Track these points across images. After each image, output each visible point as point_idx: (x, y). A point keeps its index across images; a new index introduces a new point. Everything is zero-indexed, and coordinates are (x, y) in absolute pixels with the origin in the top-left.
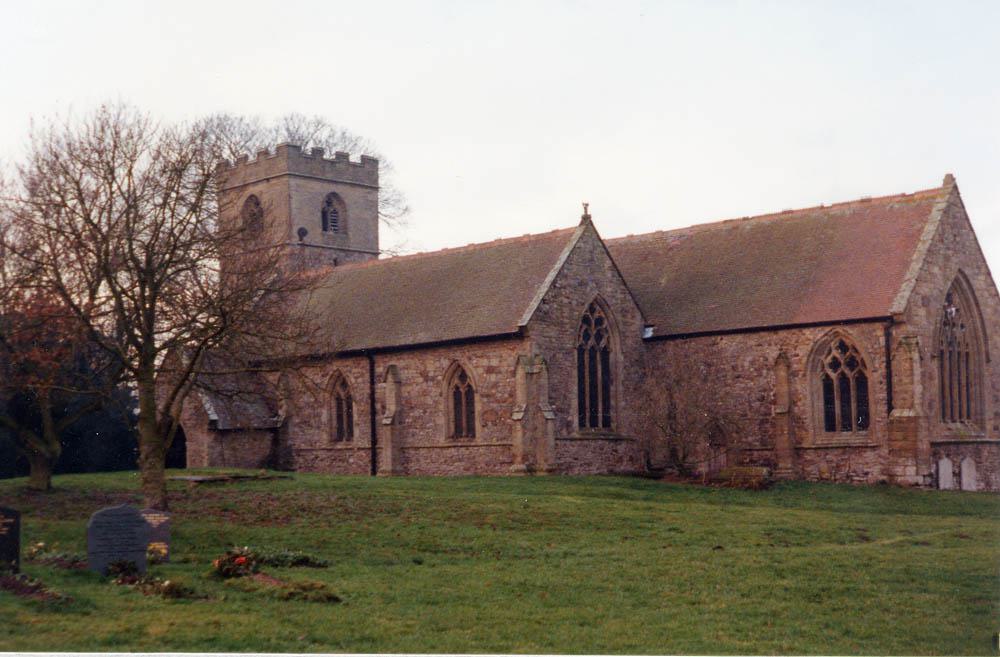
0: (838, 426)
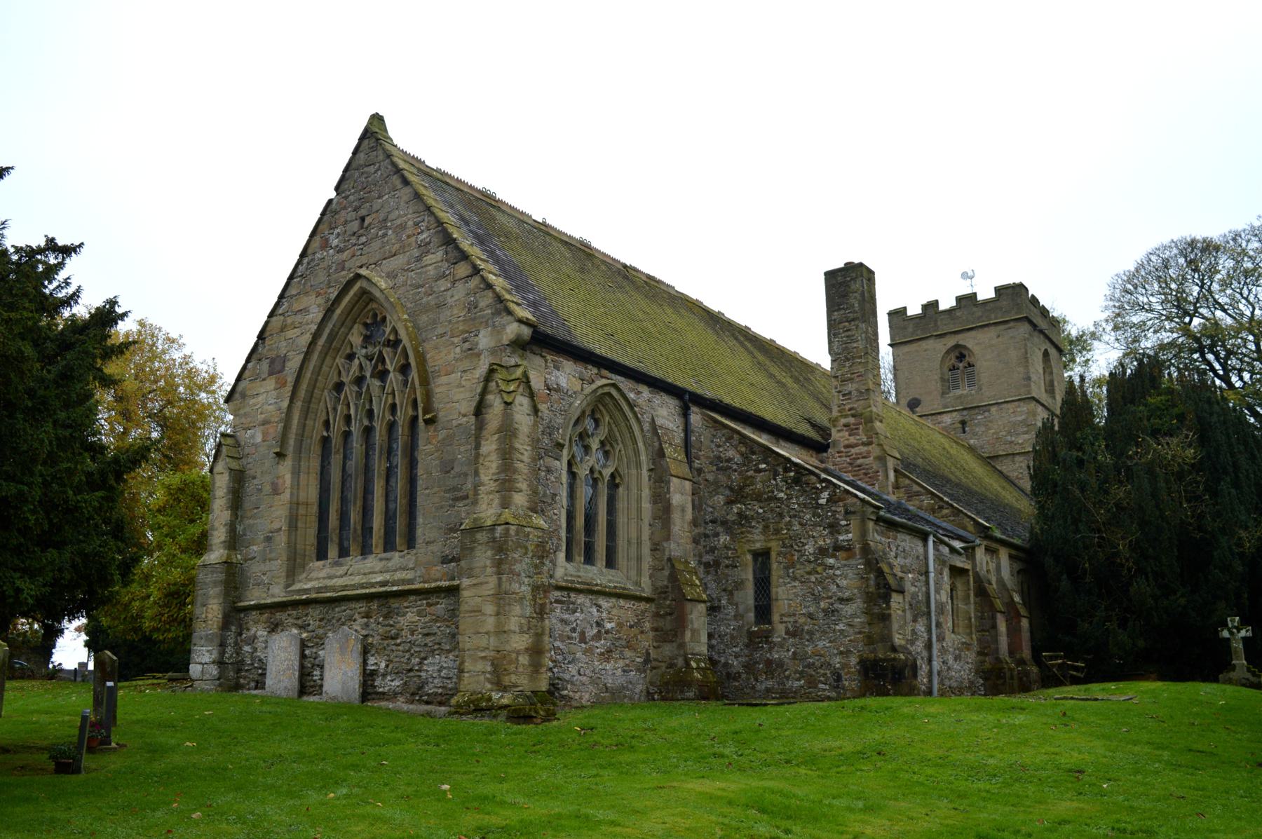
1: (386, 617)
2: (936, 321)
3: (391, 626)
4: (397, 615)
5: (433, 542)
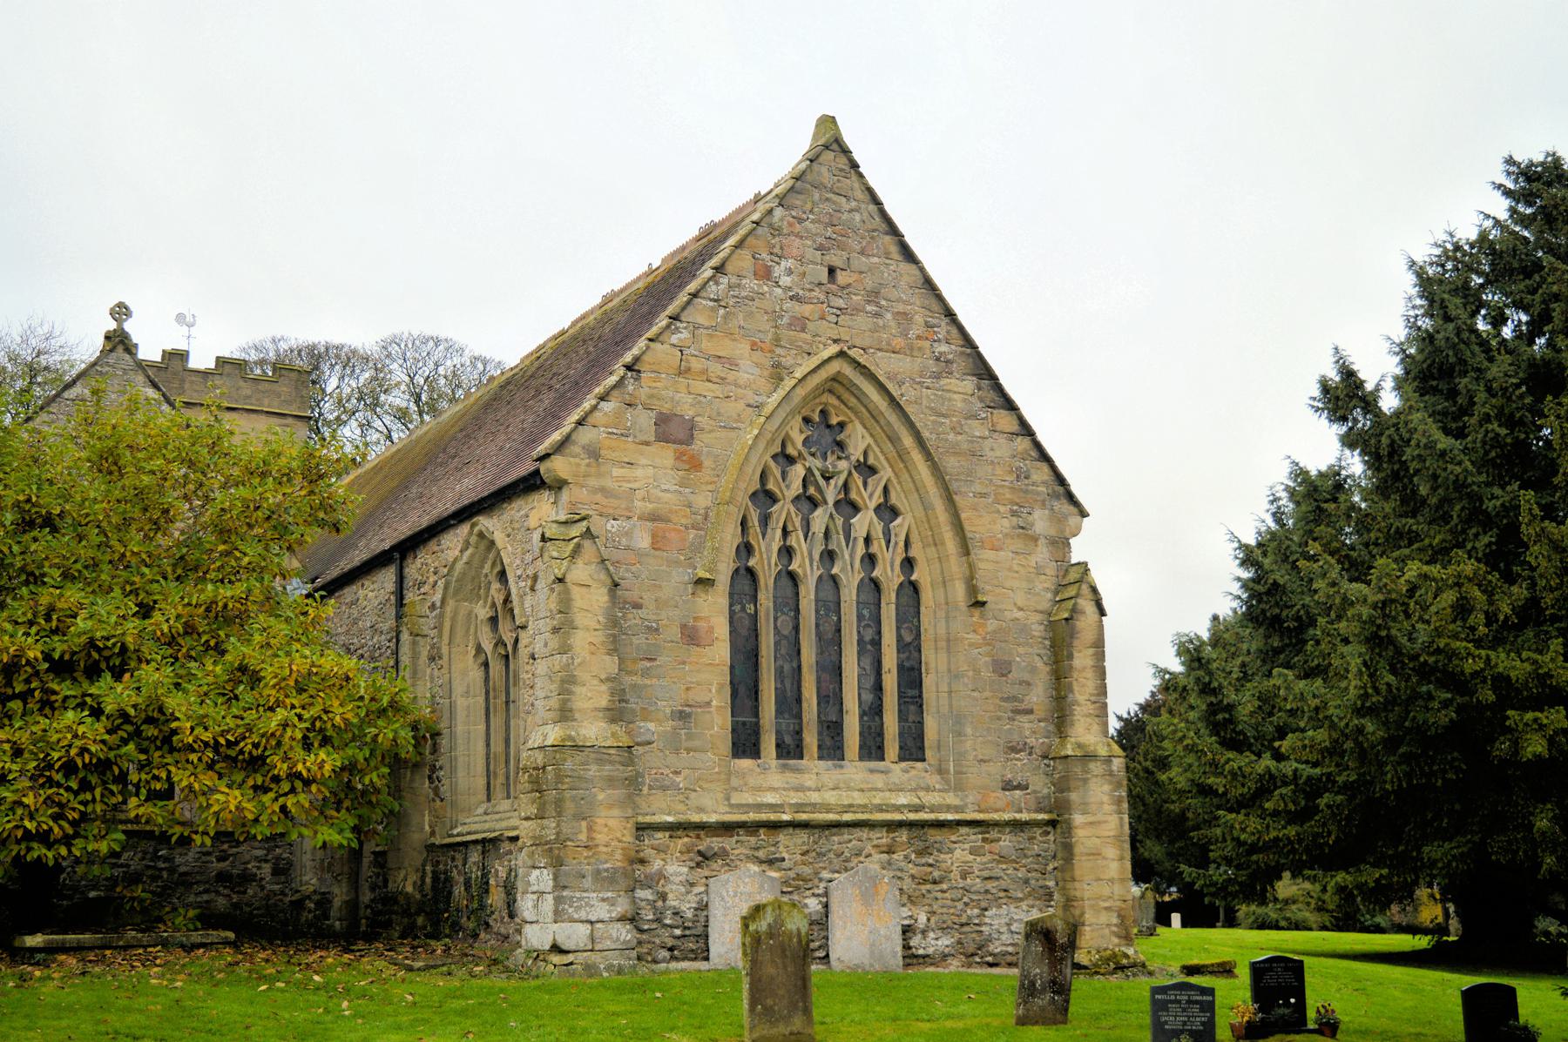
1: (920, 853)
2: (183, 381)
3: (931, 865)
4: (939, 851)
5: (989, 761)
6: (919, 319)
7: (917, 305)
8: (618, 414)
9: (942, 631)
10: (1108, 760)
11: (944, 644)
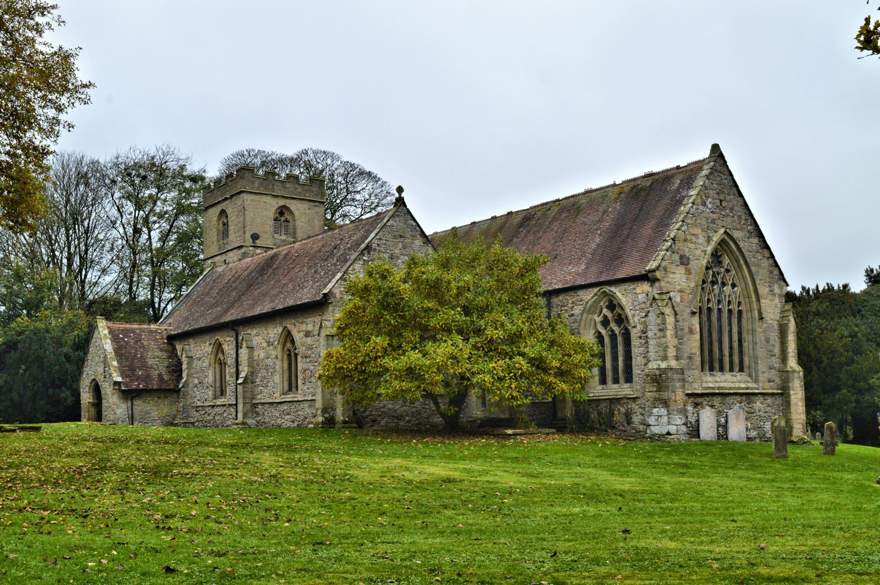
0: (622, 379)
1: (749, 404)
2: (274, 185)
6: (743, 217)
7: (739, 210)
8: (671, 256)
9: (750, 327)
10: (799, 372)
11: (751, 332)
